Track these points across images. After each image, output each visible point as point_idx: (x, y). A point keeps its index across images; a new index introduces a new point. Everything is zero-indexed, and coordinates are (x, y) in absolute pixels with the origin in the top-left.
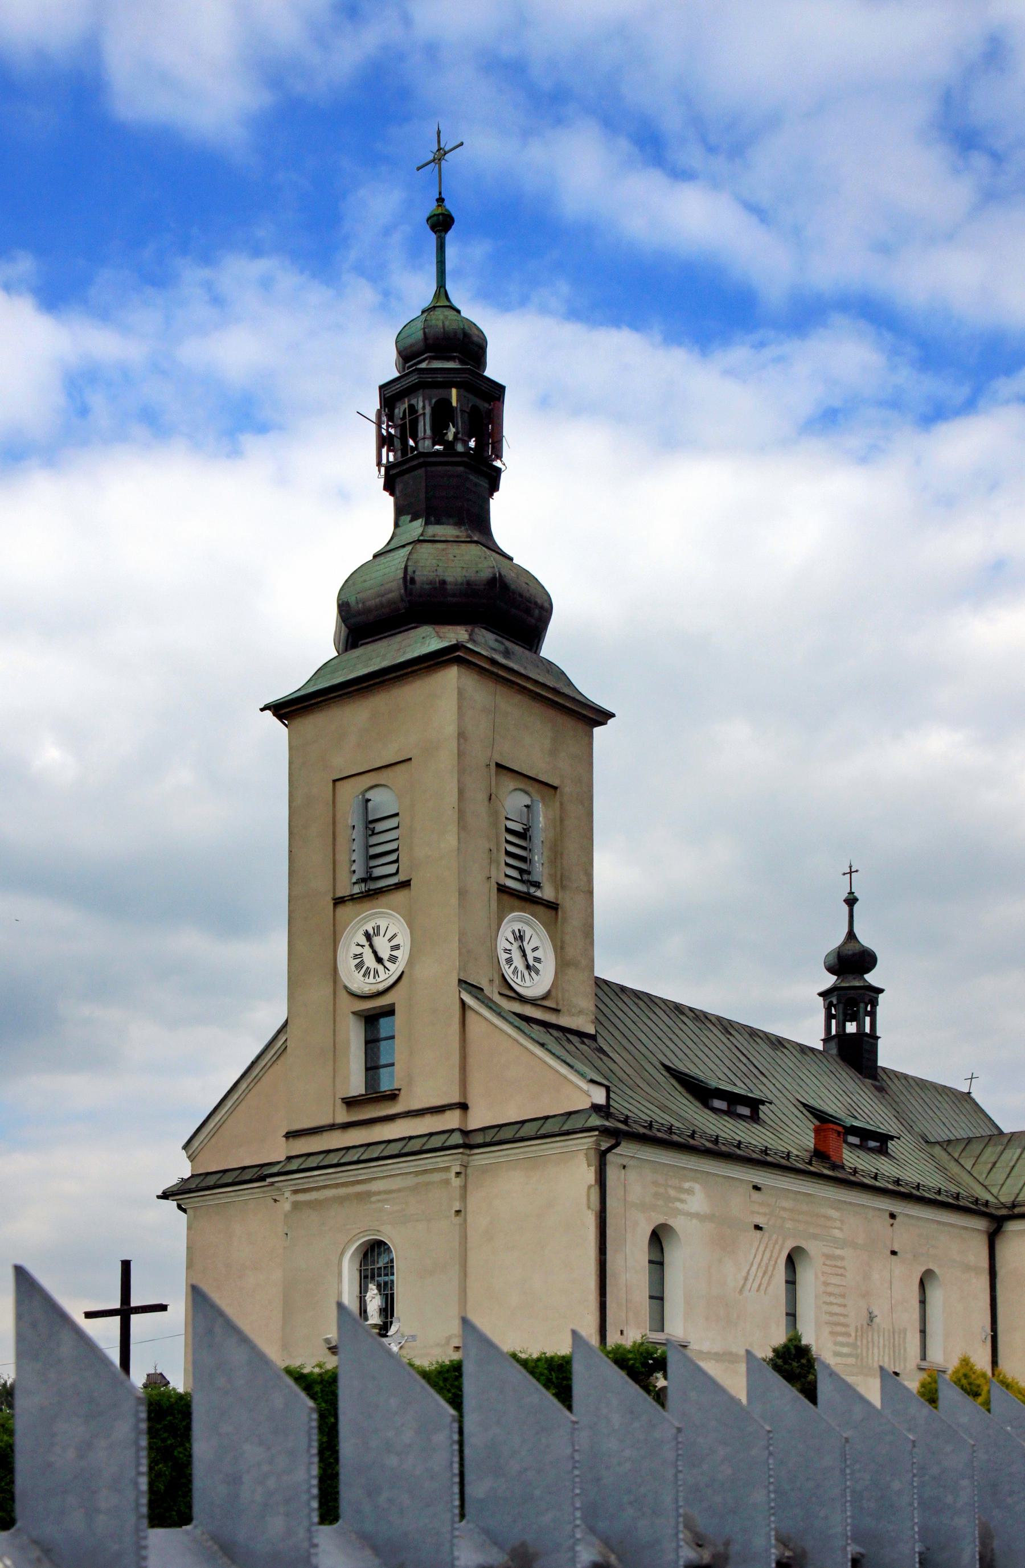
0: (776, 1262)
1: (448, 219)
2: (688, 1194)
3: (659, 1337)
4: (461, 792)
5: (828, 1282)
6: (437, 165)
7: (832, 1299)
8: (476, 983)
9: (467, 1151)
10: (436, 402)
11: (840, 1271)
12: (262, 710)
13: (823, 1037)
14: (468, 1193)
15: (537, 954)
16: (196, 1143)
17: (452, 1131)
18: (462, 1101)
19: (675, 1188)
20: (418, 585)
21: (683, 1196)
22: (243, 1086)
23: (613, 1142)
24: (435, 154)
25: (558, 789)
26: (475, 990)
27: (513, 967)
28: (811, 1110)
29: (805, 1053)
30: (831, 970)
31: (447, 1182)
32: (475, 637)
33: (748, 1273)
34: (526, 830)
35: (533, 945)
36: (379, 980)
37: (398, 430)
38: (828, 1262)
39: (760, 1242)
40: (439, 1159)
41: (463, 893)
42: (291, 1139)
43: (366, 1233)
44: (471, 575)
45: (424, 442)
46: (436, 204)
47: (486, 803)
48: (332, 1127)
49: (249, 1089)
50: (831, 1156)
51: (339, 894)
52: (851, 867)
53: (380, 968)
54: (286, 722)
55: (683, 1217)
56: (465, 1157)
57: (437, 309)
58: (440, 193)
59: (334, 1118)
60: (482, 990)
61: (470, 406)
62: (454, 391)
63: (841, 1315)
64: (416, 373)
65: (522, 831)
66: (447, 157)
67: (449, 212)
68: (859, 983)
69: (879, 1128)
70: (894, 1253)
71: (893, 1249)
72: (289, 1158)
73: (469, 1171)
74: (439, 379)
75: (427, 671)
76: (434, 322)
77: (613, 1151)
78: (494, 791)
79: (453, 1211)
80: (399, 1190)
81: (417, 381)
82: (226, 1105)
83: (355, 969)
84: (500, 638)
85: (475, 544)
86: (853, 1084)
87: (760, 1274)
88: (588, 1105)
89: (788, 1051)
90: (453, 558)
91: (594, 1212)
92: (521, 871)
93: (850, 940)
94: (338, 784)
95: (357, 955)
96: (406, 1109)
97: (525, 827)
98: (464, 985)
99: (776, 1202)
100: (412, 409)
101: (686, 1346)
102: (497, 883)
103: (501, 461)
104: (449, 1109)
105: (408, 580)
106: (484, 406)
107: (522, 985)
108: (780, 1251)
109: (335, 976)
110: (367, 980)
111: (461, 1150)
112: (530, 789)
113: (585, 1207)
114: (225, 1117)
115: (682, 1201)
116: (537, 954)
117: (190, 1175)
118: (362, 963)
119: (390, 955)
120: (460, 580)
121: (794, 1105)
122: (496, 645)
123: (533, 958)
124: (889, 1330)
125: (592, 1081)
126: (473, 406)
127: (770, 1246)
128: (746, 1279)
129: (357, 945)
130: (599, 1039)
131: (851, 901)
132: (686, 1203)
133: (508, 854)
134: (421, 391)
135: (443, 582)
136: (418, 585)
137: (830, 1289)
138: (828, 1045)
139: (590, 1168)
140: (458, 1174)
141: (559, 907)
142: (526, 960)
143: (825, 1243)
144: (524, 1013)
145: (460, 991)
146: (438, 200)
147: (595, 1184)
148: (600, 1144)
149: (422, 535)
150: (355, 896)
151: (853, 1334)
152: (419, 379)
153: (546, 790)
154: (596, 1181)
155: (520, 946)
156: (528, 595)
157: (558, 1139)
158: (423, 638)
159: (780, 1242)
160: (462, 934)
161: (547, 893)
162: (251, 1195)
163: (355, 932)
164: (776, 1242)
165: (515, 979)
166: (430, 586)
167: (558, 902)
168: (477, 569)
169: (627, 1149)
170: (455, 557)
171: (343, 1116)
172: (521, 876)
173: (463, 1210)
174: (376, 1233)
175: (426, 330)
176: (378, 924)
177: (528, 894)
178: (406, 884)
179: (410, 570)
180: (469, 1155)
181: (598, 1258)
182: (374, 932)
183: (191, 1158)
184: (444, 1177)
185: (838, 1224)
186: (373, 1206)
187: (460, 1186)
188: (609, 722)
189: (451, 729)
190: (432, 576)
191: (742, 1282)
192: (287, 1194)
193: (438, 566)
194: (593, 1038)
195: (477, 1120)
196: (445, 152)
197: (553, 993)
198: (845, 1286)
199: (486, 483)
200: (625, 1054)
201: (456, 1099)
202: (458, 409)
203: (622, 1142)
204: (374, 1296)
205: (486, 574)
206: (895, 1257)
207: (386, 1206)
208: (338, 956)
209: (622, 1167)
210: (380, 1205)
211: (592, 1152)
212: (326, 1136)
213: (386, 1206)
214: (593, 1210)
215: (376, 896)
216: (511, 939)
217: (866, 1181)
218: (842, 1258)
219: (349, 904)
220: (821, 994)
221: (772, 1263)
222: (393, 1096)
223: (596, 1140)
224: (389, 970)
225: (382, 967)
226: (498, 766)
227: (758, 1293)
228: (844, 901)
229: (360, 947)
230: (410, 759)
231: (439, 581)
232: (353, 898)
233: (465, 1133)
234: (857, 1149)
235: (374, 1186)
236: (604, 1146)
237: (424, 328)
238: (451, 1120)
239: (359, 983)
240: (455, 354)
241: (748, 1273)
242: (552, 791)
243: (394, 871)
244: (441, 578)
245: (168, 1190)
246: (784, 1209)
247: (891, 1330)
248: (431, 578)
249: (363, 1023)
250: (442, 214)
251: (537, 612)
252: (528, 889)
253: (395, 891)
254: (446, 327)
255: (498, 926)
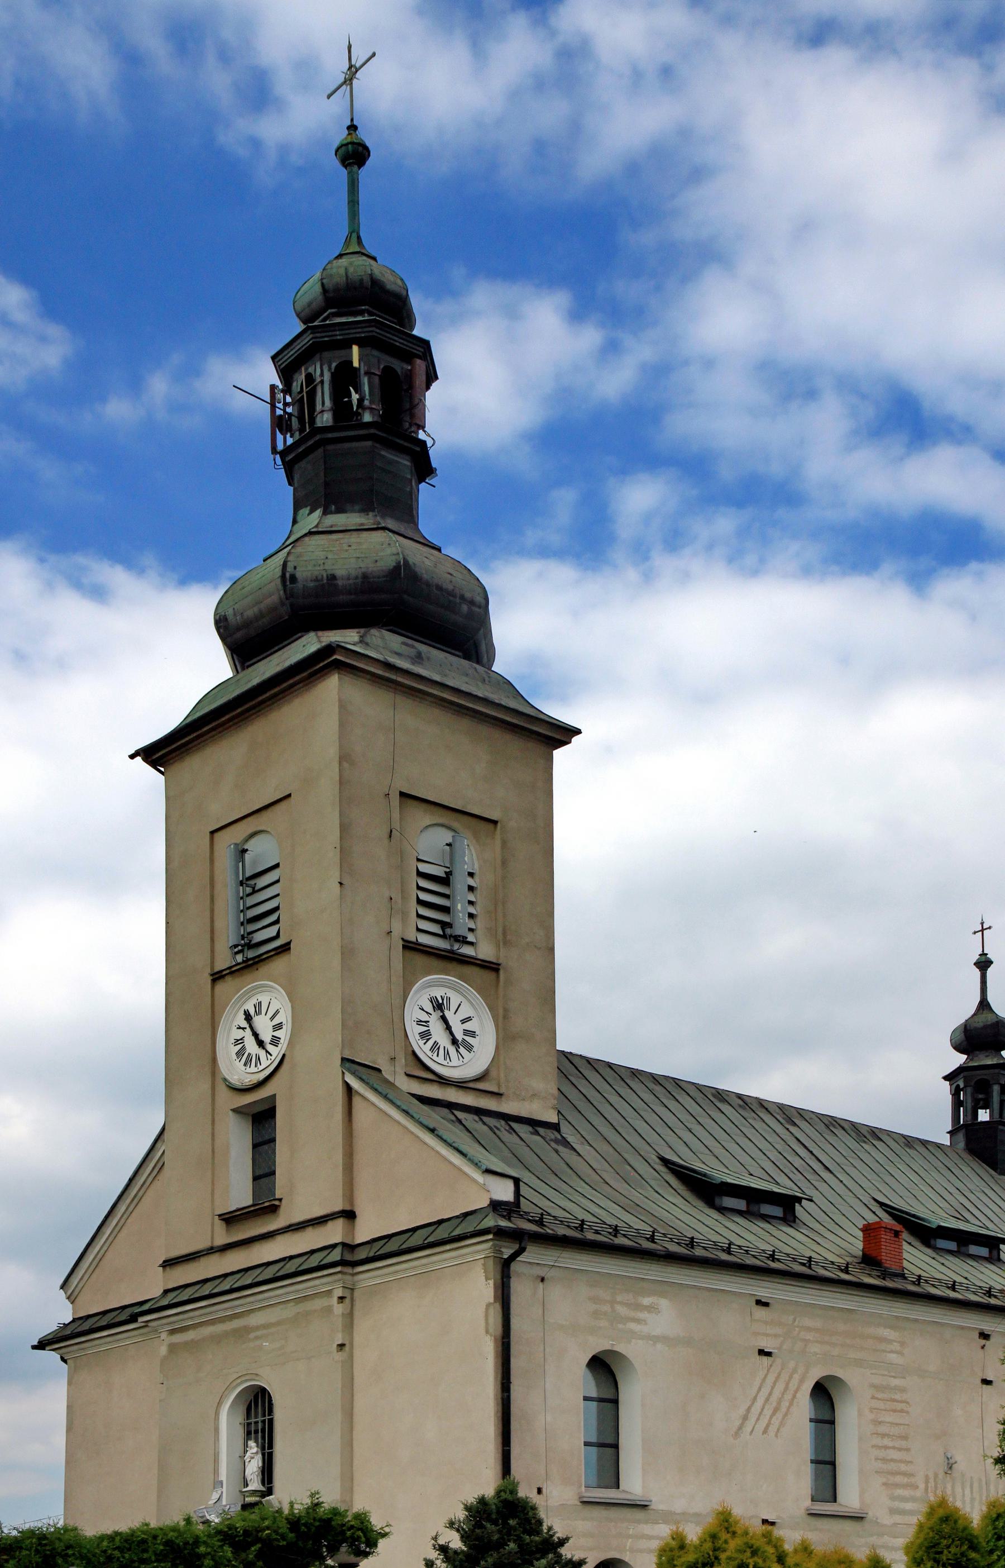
0: (794, 1396)
1: (360, 149)
2: (649, 1312)
3: (601, 1495)
4: (345, 828)
5: (880, 1420)
6: (349, 87)
7: (886, 1442)
8: (370, 1062)
9: (349, 1270)
10: (336, 367)
11: (900, 1406)
12: (132, 757)
13: (950, 1128)
14: (355, 1322)
15: (468, 1026)
16: (74, 1281)
17: (334, 1246)
18: (348, 1208)
19: (628, 1305)
20: (299, 585)
21: (642, 1315)
22: (122, 1208)
23: (517, 1246)
24: (346, 74)
25: (499, 824)
26: (366, 1071)
27: (430, 1043)
28: (889, 1210)
29: (911, 1147)
30: (958, 1048)
31: (329, 1310)
32: (368, 639)
33: (748, 1410)
34: (449, 874)
35: (463, 1014)
36: (261, 1068)
37: (296, 407)
38: (880, 1396)
39: (768, 1371)
40: (317, 1282)
41: (348, 953)
42: (168, 1269)
43: (244, 1379)
44: (368, 566)
45: (323, 415)
46: (346, 132)
47: (386, 841)
48: (211, 1251)
49: (129, 1213)
50: (883, 1261)
51: (217, 969)
52: (982, 924)
53: (262, 1053)
54: (162, 769)
55: (640, 1342)
56: (348, 1278)
57: (345, 257)
58: (352, 120)
59: (212, 1238)
60: (379, 1070)
61: (382, 367)
62: (355, 349)
63: (901, 1461)
64: (309, 332)
65: (444, 875)
66: (358, 75)
67: (362, 140)
68: (992, 1061)
69: (988, 1229)
70: (986, 1382)
71: (984, 1378)
72: (166, 1292)
73: (356, 1294)
74: (339, 337)
75: (307, 685)
76: (334, 270)
77: (518, 1259)
78: (396, 825)
79: (335, 1346)
80: (278, 1323)
81: (311, 342)
82: (104, 1233)
83: (236, 1058)
84: (410, 642)
85: (382, 531)
86: (976, 1180)
87: (768, 1412)
88: (485, 1203)
89: (915, 1152)
90: (347, 548)
91: (493, 1338)
92: (444, 925)
93: (981, 1011)
94: (217, 835)
95: (238, 1040)
96: (288, 1223)
97: (448, 870)
98: (348, 1065)
99: (794, 1320)
100: (310, 378)
101: (646, 1506)
102: (402, 939)
103: (425, 431)
104: (332, 1219)
105: (287, 578)
106: (400, 367)
107: (446, 1064)
108: (802, 1381)
109: (214, 1068)
110: (249, 1070)
111: (339, 1269)
112: (455, 825)
113: (482, 1331)
114: (105, 1248)
115: (638, 1321)
116: (468, 1026)
117: (71, 1319)
118: (243, 1048)
119: (273, 1036)
120: (353, 573)
121: (865, 1204)
122: (404, 650)
123: (463, 1031)
124: (980, 1480)
125: (488, 1171)
126: (385, 367)
127: (785, 1376)
128: (745, 1418)
129: (238, 1028)
130: (565, 1128)
131: (984, 964)
132: (646, 1324)
133: (420, 902)
134: (318, 356)
135: (333, 577)
136: (299, 585)
137: (882, 1429)
138: (955, 1137)
139: (489, 1281)
140: (341, 1299)
141: (500, 967)
142: (451, 1033)
143: (874, 1371)
144: (446, 1099)
145: (343, 1073)
146: (348, 128)
147: (495, 1301)
148: (501, 1251)
149: (316, 526)
150: (234, 969)
151: (922, 1486)
152: (314, 340)
153: (483, 825)
154: (495, 1297)
155: (441, 1017)
156: (450, 587)
157: (448, 1247)
158: (304, 646)
159: (801, 1370)
160: (347, 1003)
161: (485, 951)
162: (127, 1337)
163: (235, 1015)
164: (795, 1371)
165: (435, 1057)
166: (317, 584)
167: (500, 961)
168: (377, 558)
169: (533, 1254)
170: (350, 546)
171: (222, 1238)
172: (444, 931)
173: (347, 1343)
174: (254, 1377)
175: (324, 281)
176: (259, 1001)
177: (452, 952)
178: (286, 948)
179: (290, 569)
180: (353, 1275)
181: (499, 1396)
182: (256, 1011)
183: (72, 1298)
184: (326, 1304)
185: (896, 1346)
186: (251, 1345)
187: (343, 1314)
188: (575, 739)
189: (333, 752)
190: (318, 571)
191: (738, 1423)
192: (164, 1336)
193: (327, 558)
194: (555, 1127)
195: (365, 1231)
196: (356, 68)
197: (493, 1073)
198: (908, 1425)
199: (407, 460)
200: (603, 1147)
201: (338, 1207)
202: (362, 372)
203: (528, 1247)
204: (252, 1455)
205: (390, 563)
206: (989, 1387)
207: (265, 1344)
208: (217, 1046)
209: (540, 1279)
210: (258, 1342)
211: (491, 1263)
212: (204, 1261)
213: (265, 1344)
214: (491, 1336)
215: (255, 967)
216: (429, 1007)
217: (933, 1291)
218: (903, 1390)
219: (228, 978)
220: (946, 1078)
221: (788, 1397)
222: (273, 1209)
223: (493, 1245)
224: (271, 1055)
225: (264, 1052)
226: (402, 795)
227: (765, 1436)
228: (975, 964)
229: (241, 1030)
230: (289, 795)
231: (327, 577)
232: (233, 971)
233: (349, 1247)
234: (951, 1258)
235: (255, 1320)
236: (507, 1253)
237: (322, 279)
238: (334, 1233)
239: (240, 1074)
240: (363, 307)
241: (748, 1410)
242: (491, 826)
243: (274, 934)
244: (330, 572)
245: (44, 1339)
246: (809, 1329)
247: (984, 1480)
248: (316, 573)
249: (251, 1122)
250: (352, 143)
251: (465, 608)
252: (452, 946)
253: (276, 957)
254: (349, 274)
255: (404, 992)
